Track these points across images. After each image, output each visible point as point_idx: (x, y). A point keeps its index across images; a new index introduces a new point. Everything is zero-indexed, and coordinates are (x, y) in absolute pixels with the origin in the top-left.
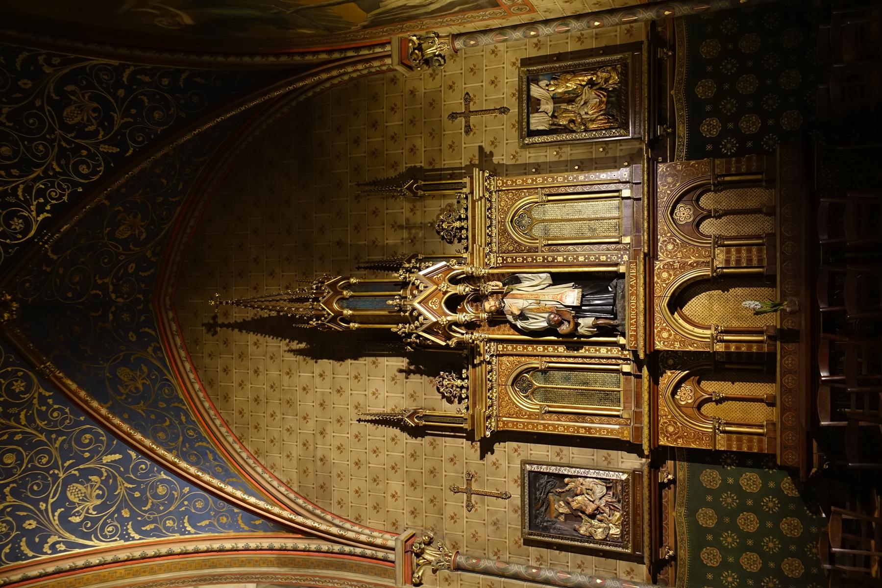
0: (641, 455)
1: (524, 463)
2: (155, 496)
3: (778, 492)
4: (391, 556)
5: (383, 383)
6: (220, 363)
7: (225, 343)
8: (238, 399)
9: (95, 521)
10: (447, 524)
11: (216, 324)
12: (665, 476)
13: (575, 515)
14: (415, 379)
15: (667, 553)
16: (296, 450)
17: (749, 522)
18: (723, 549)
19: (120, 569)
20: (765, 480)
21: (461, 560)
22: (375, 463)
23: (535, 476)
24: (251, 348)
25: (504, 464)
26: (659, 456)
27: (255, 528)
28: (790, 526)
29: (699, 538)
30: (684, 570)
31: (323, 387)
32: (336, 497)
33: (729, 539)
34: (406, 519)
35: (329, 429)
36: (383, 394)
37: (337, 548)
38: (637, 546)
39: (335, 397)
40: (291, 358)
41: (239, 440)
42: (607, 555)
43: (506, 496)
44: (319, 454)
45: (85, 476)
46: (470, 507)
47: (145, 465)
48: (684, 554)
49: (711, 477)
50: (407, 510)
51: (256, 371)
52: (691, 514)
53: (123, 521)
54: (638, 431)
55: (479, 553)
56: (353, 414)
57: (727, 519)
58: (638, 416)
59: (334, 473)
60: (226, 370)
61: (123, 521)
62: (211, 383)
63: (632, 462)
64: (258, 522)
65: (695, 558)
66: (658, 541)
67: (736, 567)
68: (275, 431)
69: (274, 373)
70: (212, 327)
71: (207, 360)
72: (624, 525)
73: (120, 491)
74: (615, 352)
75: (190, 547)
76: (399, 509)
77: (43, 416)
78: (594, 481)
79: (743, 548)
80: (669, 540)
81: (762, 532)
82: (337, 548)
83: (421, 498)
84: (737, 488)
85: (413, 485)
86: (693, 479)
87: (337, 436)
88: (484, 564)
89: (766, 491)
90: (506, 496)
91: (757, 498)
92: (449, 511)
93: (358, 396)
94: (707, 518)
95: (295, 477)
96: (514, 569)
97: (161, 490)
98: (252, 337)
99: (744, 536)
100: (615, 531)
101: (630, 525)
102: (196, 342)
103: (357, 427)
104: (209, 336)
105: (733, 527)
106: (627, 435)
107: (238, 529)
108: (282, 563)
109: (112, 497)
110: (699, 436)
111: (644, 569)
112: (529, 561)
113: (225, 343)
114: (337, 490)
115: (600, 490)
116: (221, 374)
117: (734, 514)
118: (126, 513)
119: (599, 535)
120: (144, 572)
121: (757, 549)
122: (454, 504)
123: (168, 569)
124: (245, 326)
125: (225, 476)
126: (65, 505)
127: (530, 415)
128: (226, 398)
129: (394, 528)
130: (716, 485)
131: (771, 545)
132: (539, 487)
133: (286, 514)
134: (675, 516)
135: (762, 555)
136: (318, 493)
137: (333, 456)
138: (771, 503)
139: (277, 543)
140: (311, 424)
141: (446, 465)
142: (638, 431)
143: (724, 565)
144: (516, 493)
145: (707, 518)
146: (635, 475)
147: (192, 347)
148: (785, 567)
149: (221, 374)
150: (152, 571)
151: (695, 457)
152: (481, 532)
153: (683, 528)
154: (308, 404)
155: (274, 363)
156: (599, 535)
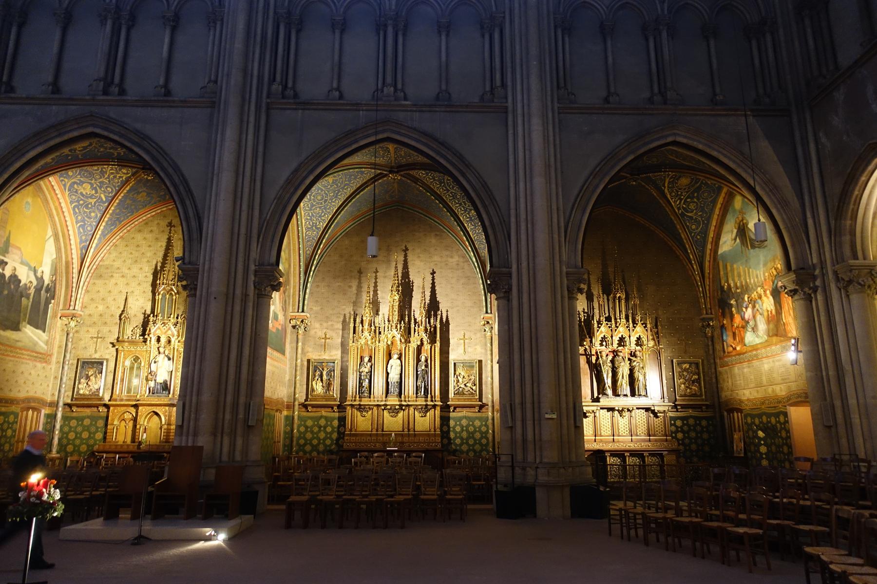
0: (110, 400)
1: (107, 360)
2: (90, 212)
3: (95, 444)
4: (71, 308)
5: (140, 304)
6: (155, 228)
7: (163, 231)
8: (139, 236)
9: (76, 192)
10: (85, 329)
11: (171, 226)
12: (101, 409)
13: (88, 377)
14: (142, 317)
15: (74, 409)
16: (117, 264)
17: (85, 435)
18: (76, 427)
19: (57, 204)
20: (100, 440)
21: (71, 335)
22: (110, 299)
23: (102, 363)
24: (160, 244)
25: (107, 351)
26: (107, 406)
27: (81, 250)
28: (84, 448)
29: (80, 419)
30: (69, 414)
31: (141, 277)
32: (97, 282)
33: (79, 429)
34: (87, 312)
35: (124, 279)
36: (137, 303)
37: (74, 285)
38: (76, 399)
39: (137, 282)
40: (154, 263)
41: (121, 237)
42: (74, 388)
43: (96, 352)
44: (115, 275)
45: (93, 188)
46: (92, 338)
47: (102, 208)
48: (74, 414)
49: (101, 423)
50: (91, 312)
51: (150, 246)
52: (88, 417)
53: (78, 201)
54: (116, 400)
55: (74, 341)
56: (130, 291)
57: (87, 429)
58: (122, 400)
59: (107, 282)
60: (151, 231)
61: (78, 201)
62: (146, 224)
63: (107, 397)
64: (84, 252)
65: (73, 418)
66: (78, 406)
67: (70, 431)
68: (125, 254)
69: (149, 254)
70: (170, 225)
71: (156, 222)
72: (84, 395)
73: (90, 200)
74: (143, 392)
75: (70, 228)
76: (91, 309)
77: (115, 177)
78: (99, 385)
79: (76, 433)
80: (79, 409)
81: (82, 439)
82: (74, 285)
83: (95, 318)
84: (97, 431)
85: (101, 315)
86: (101, 418)
87: (122, 282)
88: (70, 344)
89: (96, 440)
90: (96, 352)
91: (93, 438)
92: (90, 329)
93: (137, 293)
94: (87, 422)
95: (106, 263)
96: (68, 356)
97: (93, 214)
98: (164, 244)
99: (81, 434)
100: (81, 392)
101: (84, 397)
102: (165, 217)
103: (124, 291)
104: (166, 223)
105: (83, 430)
106: (114, 396)
107: (80, 243)
108: (67, 263)
109: (87, 197)
110: (113, 420)
111: (69, 401)
112: (71, 360)
113: (163, 231)
114: (99, 282)
115: (96, 387)
116: (150, 229)
117: (88, 430)
118: (81, 202)
119: (80, 386)
120: (57, 212)
121: (76, 437)
122: (93, 331)
123: (60, 220)
124: (169, 240)
125: (103, 235)
126: (81, 183)
127: (124, 362)
128: (140, 231)
129: (84, 307)
130: (98, 425)
131: (78, 442)
132: (98, 364)
133: (89, 260)
134: (88, 411)
135: (74, 439)
136: (98, 275)
137: (113, 281)
138: (91, 442)
139: (75, 256)
140: (127, 271)
141: (108, 329)
142: (116, 400)
143: (71, 427)
144: (97, 356)
145: (87, 422)
146: (101, 399)
147: (163, 215)
148: (70, 446)
149: (150, 229)
150: (58, 215)
151: (135, 420)
152: (83, 342)
153: (84, 415)
154: (135, 270)
155: (153, 254)
156: (80, 386)
